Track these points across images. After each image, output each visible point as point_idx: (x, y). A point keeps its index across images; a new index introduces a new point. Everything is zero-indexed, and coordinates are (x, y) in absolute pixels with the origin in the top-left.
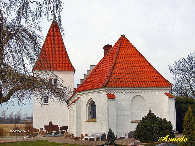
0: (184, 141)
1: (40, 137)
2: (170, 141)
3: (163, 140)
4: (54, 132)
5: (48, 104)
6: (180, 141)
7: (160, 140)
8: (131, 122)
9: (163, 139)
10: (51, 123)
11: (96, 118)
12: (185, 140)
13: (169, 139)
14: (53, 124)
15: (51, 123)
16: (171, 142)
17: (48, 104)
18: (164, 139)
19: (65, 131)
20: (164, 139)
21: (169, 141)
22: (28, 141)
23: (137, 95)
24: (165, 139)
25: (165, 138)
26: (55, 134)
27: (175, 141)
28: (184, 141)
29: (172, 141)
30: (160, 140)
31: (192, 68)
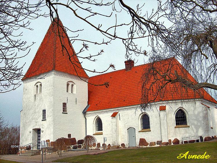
0: (205, 158)
1: (148, 146)
2: (191, 158)
3: (182, 157)
4: (73, 146)
5: (67, 113)
6: (201, 158)
7: (179, 157)
8: (139, 132)
9: (182, 155)
10: (69, 135)
11: (149, 128)
12: (206, 157)
13: (189, 155)
15: (69, 135)
16: (191, 159)
17: (67, 113)
18: (183, 156)
19: (82, 145)
20: (183, 156)
21: (189, 158)
22: (109, 150)
23: (71, 81)
24: (185, 156)
25: (184, 155)
26: (74, 148)
27: (195, 158)
28: (206, 158)
29: (193, 158)
30: (179, 157)
31: (186, 26)
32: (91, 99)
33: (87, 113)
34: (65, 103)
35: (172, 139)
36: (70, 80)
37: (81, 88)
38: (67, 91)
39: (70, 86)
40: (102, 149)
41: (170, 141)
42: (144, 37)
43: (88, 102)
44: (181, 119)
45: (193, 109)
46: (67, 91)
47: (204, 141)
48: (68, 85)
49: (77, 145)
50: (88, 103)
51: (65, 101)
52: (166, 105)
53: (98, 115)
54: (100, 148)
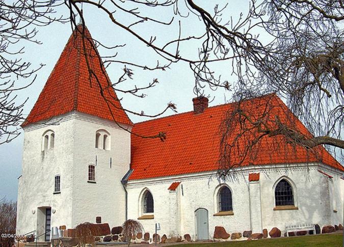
4: (104, 237)
5: (95, 183)
10: (99, 219)
14: (103, 222)
15: (99, 219)
17: (95, 183)
26: (105, 240)
33: (128, 183)
34: (92, 166)
36: (102, 127)
37: (119, 142)
38: (97, 147)
39: (101, 138)
43: (131, 165)
44: (284, 195)
45: (305, 180)
46: (97, 147)
47: (322, 233)
48: (98, 136)
49: (111, 235)
51: (93, 163)
53: (147, 187)
54: (149, 241)
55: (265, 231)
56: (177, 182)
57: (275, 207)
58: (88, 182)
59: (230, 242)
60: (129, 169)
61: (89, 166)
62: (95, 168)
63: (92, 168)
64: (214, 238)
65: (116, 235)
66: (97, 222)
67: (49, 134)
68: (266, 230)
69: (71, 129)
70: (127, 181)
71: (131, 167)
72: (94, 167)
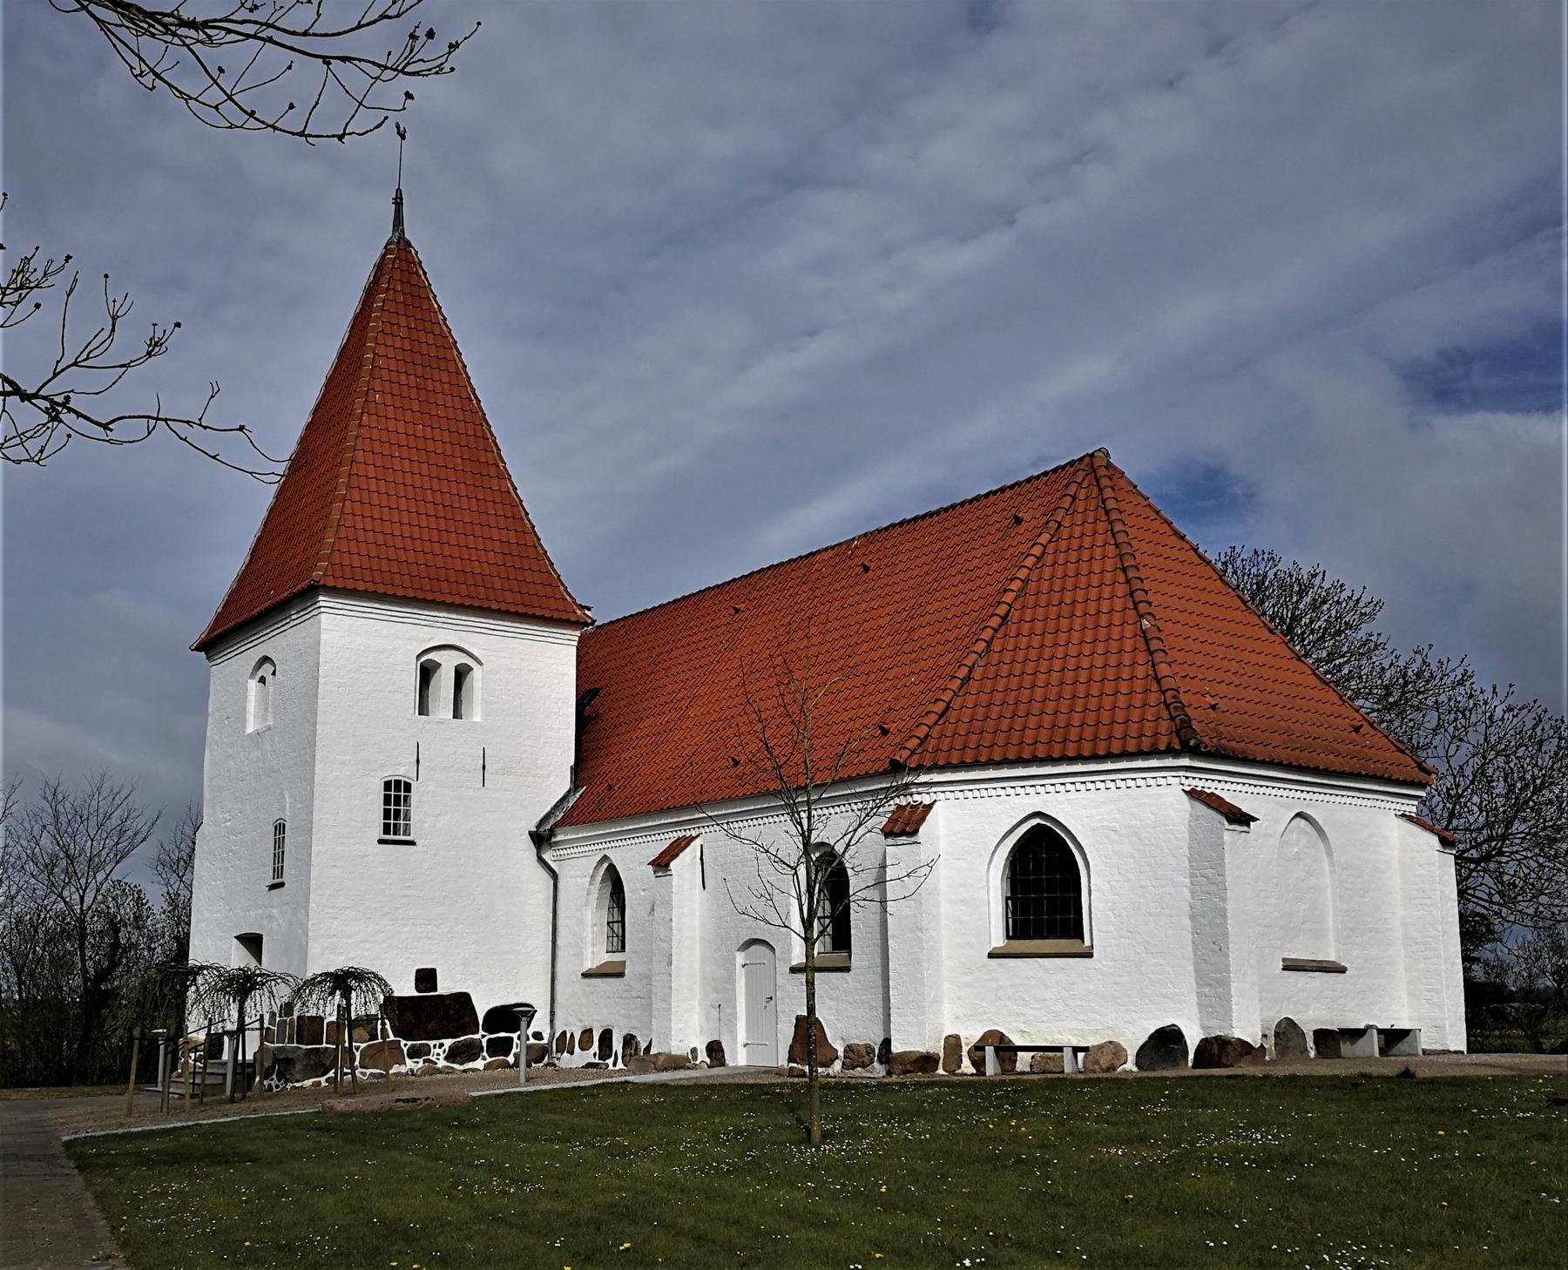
4: (448, 1042)
5: (412, 843)
10: (426, 978)
14: (445, 987)
15: (426, 978)
17: (412, 843)
26: (452, 1055)
32: (592, 745)
33: (559, 838)
34: (398, 783)
35: (970, 1035)
36: (255, 654)
37: (531, 678)
38: (423, 709)
39: (444, 682)
40: (620, 1065)
41: (953, 1043)
42: (11, 383)
43: (576, 770)
44: (1044, 892)
45: (1123, 819)
46: (423, 709)
47: (1194, 1067)
48: (427, 673)
49: (482, 1037)
50: (579, 772)
51: (404, 772)
52: (934, 797)
53: (607, 852)
54: (610, 1061)
55: (953, 1043)
56: (688, 834)
57: (998, 940)
58: (381, 842)
59: (1139, 1080)
60: (561, 783)
61: (387, 785)
62: (414, 794)
63: (398, 789)
64: (790, 1060)
65: (502, 1034)
66: (418, 989)
67: (448, 663)
68: (957, 1038)
69: (356, 646)
70: (552, 832)
71: (576, 785)
72: (408, 787)
